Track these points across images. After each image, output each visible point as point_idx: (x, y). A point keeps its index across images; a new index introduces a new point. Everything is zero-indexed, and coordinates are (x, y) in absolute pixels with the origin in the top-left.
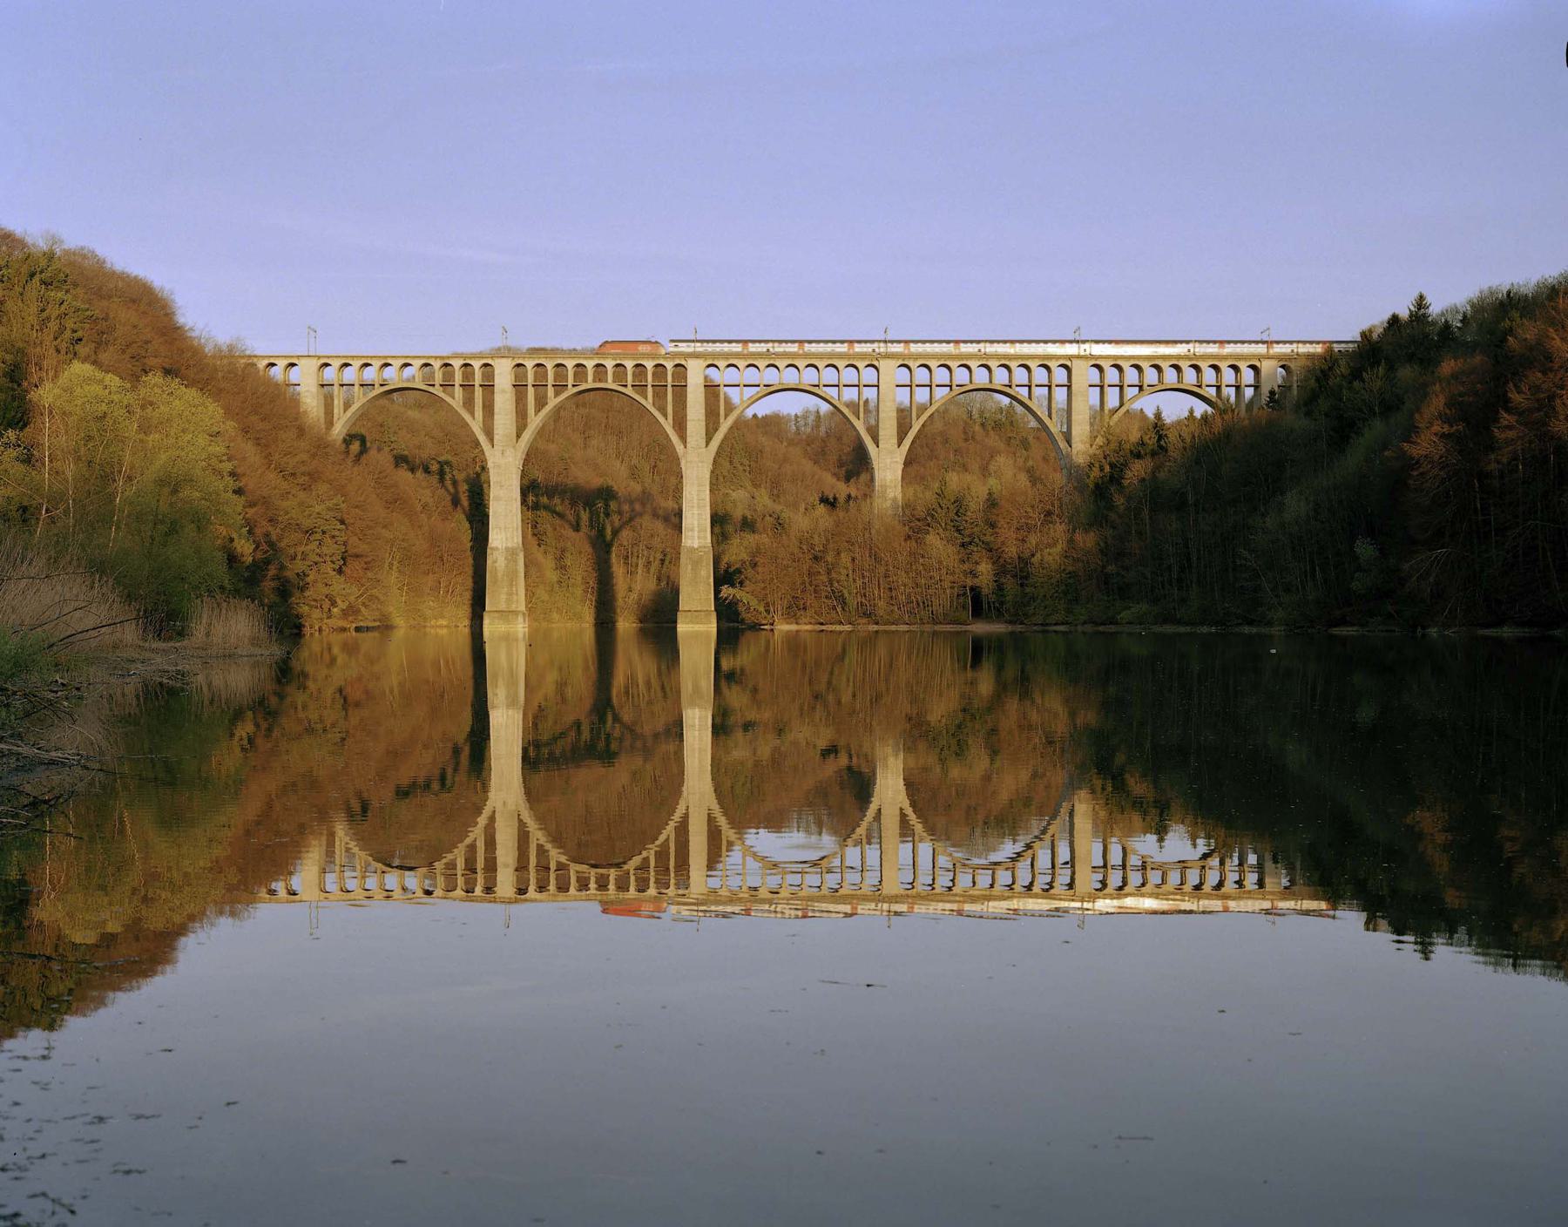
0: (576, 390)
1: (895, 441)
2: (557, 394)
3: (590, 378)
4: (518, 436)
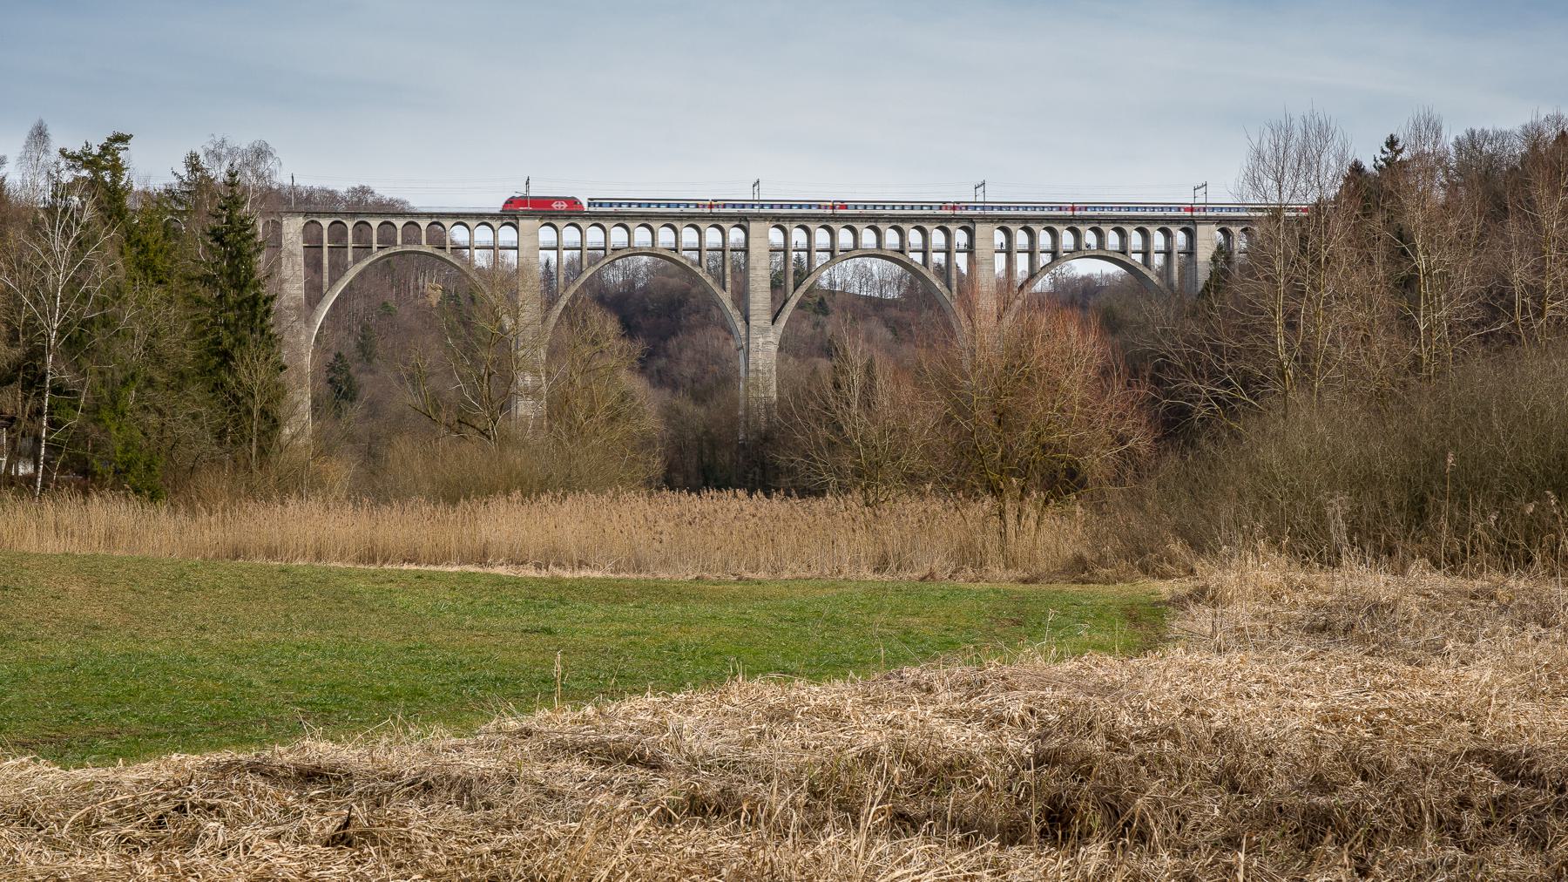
0: (381, 254)
1: (769, 317)
2: (356, 260)
3: (399, 241)
4: (544, 320)
